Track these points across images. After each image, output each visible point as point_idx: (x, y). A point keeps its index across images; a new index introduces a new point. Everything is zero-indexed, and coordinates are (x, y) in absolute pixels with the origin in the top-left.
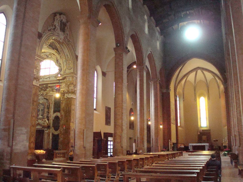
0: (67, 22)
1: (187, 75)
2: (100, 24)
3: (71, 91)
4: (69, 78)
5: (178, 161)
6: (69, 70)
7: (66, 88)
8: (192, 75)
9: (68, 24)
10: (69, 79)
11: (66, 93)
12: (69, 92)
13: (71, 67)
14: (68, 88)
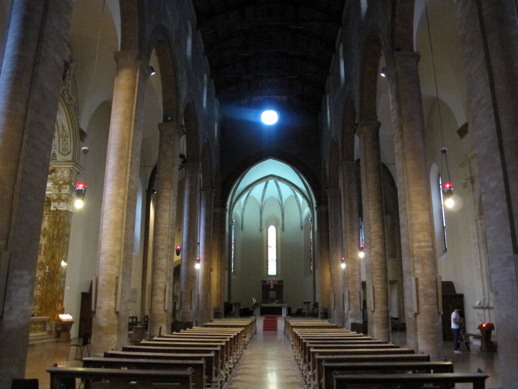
0: (71, 62)
1: (250, 189)
2: (153, 74)
3: (67, 197)
4: (62, 172)
5: (323, 341)
6: (63, 156)
7: (54, 190)
8: (260, 187)
9: (72, 65)
10: (61, 174)
11: (55, 201)
12: (61, 199)
13: (69, 150)
14: (60, 191)
